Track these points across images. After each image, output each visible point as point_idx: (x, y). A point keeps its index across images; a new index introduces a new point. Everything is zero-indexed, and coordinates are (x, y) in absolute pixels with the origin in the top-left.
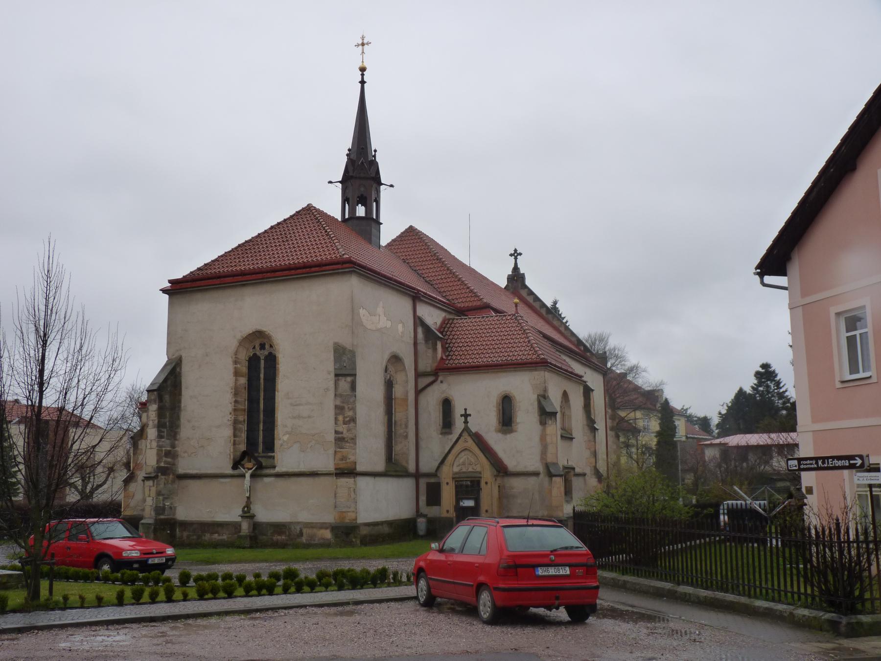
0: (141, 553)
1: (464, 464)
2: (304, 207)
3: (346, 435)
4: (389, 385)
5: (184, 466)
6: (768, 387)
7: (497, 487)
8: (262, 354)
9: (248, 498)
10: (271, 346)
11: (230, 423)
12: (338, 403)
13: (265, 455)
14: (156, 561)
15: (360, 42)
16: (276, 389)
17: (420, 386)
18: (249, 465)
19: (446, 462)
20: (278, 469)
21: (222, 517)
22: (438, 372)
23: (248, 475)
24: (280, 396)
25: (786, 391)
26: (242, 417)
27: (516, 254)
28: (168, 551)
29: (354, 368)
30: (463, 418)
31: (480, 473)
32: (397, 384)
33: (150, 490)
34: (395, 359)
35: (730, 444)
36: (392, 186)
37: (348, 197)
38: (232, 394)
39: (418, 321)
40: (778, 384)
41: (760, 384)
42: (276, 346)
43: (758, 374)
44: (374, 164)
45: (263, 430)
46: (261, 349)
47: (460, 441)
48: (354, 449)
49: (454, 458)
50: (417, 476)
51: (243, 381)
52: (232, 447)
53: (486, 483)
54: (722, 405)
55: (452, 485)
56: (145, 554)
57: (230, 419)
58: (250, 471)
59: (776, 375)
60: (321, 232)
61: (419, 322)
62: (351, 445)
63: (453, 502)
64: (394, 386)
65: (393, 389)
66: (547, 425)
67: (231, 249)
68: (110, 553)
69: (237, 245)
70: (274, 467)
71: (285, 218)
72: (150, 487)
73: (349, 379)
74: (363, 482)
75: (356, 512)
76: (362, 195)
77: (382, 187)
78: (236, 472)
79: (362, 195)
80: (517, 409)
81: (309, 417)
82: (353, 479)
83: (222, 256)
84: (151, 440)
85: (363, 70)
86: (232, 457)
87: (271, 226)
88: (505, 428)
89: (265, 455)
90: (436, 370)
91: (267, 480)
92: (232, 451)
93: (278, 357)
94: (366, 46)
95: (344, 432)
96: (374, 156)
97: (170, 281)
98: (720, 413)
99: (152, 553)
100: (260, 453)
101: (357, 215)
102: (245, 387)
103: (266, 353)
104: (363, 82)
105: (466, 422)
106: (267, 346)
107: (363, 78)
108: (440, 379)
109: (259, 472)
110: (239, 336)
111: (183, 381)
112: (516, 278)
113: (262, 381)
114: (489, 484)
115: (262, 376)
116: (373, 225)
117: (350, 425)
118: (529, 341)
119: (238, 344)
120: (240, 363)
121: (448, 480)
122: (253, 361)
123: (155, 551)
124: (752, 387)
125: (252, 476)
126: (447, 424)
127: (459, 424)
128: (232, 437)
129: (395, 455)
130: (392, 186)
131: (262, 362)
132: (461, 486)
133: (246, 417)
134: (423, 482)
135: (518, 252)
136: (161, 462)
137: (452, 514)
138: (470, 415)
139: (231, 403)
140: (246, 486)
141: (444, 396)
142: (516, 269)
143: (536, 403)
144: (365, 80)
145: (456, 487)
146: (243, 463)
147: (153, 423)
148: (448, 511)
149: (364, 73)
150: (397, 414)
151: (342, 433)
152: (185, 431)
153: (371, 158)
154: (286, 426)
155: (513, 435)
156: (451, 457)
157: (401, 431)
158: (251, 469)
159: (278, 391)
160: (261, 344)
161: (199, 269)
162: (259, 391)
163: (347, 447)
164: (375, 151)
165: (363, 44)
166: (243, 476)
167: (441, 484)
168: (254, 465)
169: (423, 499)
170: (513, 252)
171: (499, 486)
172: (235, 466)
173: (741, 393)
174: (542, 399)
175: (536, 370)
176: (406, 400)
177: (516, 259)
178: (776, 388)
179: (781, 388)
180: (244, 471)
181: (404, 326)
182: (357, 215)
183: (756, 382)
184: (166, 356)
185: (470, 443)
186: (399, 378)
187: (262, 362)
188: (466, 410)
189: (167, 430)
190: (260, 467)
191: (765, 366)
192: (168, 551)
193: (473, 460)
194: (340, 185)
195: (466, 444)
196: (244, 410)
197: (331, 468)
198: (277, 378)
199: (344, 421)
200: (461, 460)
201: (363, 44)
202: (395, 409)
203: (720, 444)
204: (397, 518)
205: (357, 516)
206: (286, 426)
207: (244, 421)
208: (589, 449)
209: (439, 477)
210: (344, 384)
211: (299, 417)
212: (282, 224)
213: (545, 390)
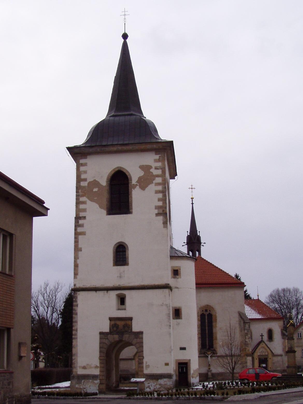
8: (206, 313)
10: (210, 311)
15: (191, 187)
31: (268, 355)
46: (205, 311)
53: (270, 359)
58: (210, 355)
70: (217, 354)
73: (248, 324)
85: (192, 199)
87: (218, 267)
103: (208, 313)
104: (192, 204)
105: (262, 338)
106: (208, 311)
107: (192, 202)
113: (207, 323)
121: (256, 358)
125: (211, 357)
138: (263, 336)
149: (193, 200)
160: (205, 310)
164: (199, 232)
165: (192, 188)
166: (208, 357)
188: (262, 334)
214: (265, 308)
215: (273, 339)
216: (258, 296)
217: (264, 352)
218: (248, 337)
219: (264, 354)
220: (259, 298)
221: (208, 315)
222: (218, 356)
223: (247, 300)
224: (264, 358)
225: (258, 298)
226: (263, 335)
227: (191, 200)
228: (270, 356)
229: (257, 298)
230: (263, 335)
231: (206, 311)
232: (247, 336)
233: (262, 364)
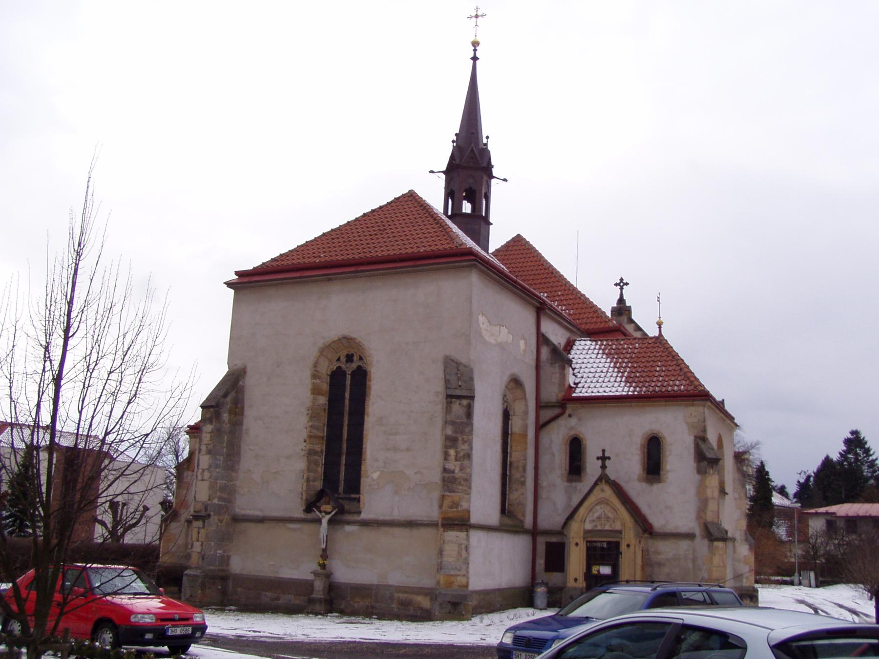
0: (157, 620)
2: (404, 193)
3: (458, 474)
4: (506, 416)
5: (244, 505)
6: (856, 454)
7: (641, 552)
9: (324, 550)
10: (361, 358)
11: (304, 453)
12: (449, 431)
13: (347, 496)
14: (179, 631)
15: (474, 14)
16: (366, 412)
17: (542, 420)
18: (328, 508)
19: (576, 516)
20: (364, 516)
21: (289, 572)
22: (565, 404)
23: (325, 521)
24: (370, 422)
25: (876, 459)
26: (319, 446)
27: (622, 284)
28: (196, 617)
29: (472, 389)
30: (600, 461)
31: (620, 532)
32: (514, 415)
33: (199, 533)
34: (516, 382)
35: (839, 514)
36: (505, 180)
37: (453, 189)
38: (308, 417)
39: (541, 339)
40: (867, 451)
41: (848, 452)
42: (368, 358)
43: (847, 442)
44: (485, 153)
45: (345, 465)
46: (347, 361)
47: (595, 492)
48: (468, 494)
49: (587, 511)
50: (534, 533)
51: (323, 400)
52: (305, 484)
53: (628, 546)
55: (583, 547)
56: (162, 620)
57: (304, 448)
58: (328, 517)
59: (866, 443)
60: (428, 221)
61: (542, 339)
62: (465, 488)
63: (583, 568)
64: (511, 417)
65: (510, 422)
66: (707, 475)
67: (313, 238)
68: (114, 617)
69: (321, 234)
70: (360, 513)
71: (381, 205)
72: (199, 528)
73: (465, 402)
74: (477, 538)
75: (466, 576)
76: (470, 188)
77: (493, 181)
78: (310, 516)
79: (470, 188)
81: (408, 450)
82: (465, 533)
83: (302, 246)
84: (203, 470)
85: (475, 44)
86: (304, 497)
88: (650, 476)
89: (347, 496)
90: (563, 400)
91: (348, 528)
92: (305, 489)
93: (370, 372)
94: (480, 18)
95: (456, 471)
96: (486, 145)
97: (237, 273)
98: (799, 482)
99: (173, 620)
100: (340, 494)
101: (464, 211)
102: (325, 410)
103: (354, 366)
104: (475, 59)
105: (604, 467)
106: (355, 358)
107: (475, 54)
108: (568, 412)
109: (339, 517)
110: (320, 343)
111: (246, 397)
112: (622, 309)
113: (347, 402)
114: (632, 547)
115: (347, 395)
116: (482, 223)
117: (464, 463)
118: (681, 369)
119: (319, 354)
122: (337, 376)
123: (177, 617)
124: (841, 454)
125: (330, 522)
127: (592, 468)
128: (306, 472)
129: (508, 505)
130: (505, 180)
131: (349, 377)
132: (595, 548)
133: (324, 447)
134: (542, 541)
135: (624, 281)
136: (214, 499)
137: (582, 584)
138: (609, 458)
139: (306, 428)
140: (322, 535)
141: (572, 433)
142: (621, 300)
143: (692, 446)
144: (477, 56)
145: (588, 549)
146: (318, 504)
147: (207, 447)
148: (576, 580)
149: (477, 48)
151: (453, 472)
152: (247, 462)
153: (482, 146)
154: (377, 460)
155: (660, 485)
156: (582, 510)
157: (516, 475)
158: (329, 513)
159: (368, 416)
161: (273, 260)
162: (342, 415)
163: (460, 491)
164: (487, 138)
165: (477, 16)
167: (566, 545)
168: (334, 508)
169: (541, 562)
170: (618, 281)
171: (642, 551)
172: (309, 509)
173: (827, 462)
174: (700, 442)
175: (693, 405)
176: (525, 436)
177: (622, 289)
178: (865, 455)
179: (871, 455)
180: (321, 516)
181: (526, 343)
182: (464, 211)
183: (845, 448)
184: (227, 365)
185: (608, 492)
186: (518, 408)
187: (349, 377)
188: (604, 451)
189: (223, 457)
190: (342, 511)
191: (855, 433)
192: (196, 617)
193: (610, 515)
194: (443, 176)
195: (602, 495)
196: (323, 438)
197: (434, 513)
198: (367, 399)
199: (456, 456)
200: (596, 515)
201: (477, 16)
202: (511, 447)
203: (827, 513)
204: (510, 585)
205: (468, 583)
206: (377, 460)
207: (322, 452)
208: (740, 509)
209: (566, 535)
210: (458, 408)
211: (395, 449)
212: (377, 212)
213: (704, 430)
214: (663, 363)
215: (662, 473)
216: (660, 325)
217: (608, 518)
218: (456, 452)
219: (607, 528)
220: (663, 333)
221: (353, 374)
222: (366, 524)
223: (617, 340)
224: (608, 543)
225: (660, 331)
226: (606, 455)
227: (473, 48)
228: (630, 536)
229: (657, 334)
230: (606, 455)
231: (350, 358)
232: (456, 448)
233: (600, 564)
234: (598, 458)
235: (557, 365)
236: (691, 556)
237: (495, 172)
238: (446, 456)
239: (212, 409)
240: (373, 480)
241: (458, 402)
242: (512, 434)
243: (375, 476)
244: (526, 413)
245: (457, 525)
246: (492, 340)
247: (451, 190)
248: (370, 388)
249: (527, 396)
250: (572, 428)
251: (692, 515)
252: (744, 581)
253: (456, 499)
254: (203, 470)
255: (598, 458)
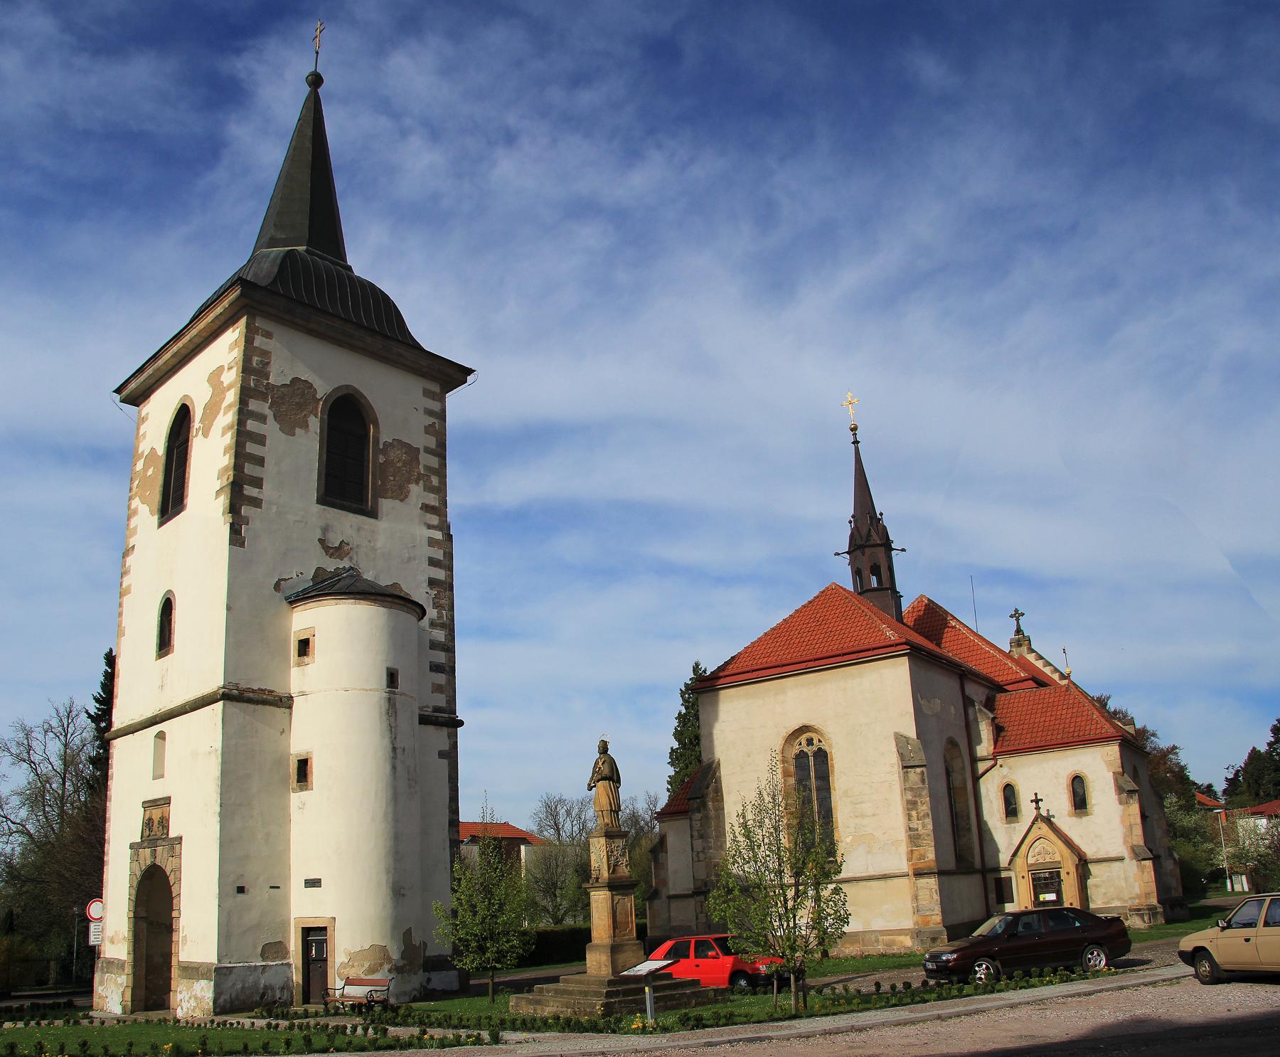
1: (1039, 854)
8: (809, 750)
20: (843, 875)
36: (903, 550)
46: (808, 745)
53: (1068, 873)
54: (1227, 769)
80: (1091, 790)
81: (874, 815)
104: (856, 442)
105: (1038, 808)
108: (1000, 762)
120: (787, 762)
126: (1011, 811)
127: (1027, 811)
130: (903, 550)
131: (811, 759)
132: (1039, 879)
141: (1005, 781)
150: (957, 805)
156: (1024, 847)
160: (807, 740)
164: (881, 514)
173: (1254, 754)
177: (1018, 620)
187: (811, 759)
188: (1036, 794)
195: (1040, 833)
200: (1037, 850)
211: (863, 816)
234: (1032, 801)
235: (984, 722)
236: (1123, 876)
237: (893, 546)
238: (909, 817)
239: (698, 800)
240: (847, 844)
241: (912, 770)
242: (954, 788)
243: (848, 840)
244: (963, 769)
245: (926, 874)
246: (930, 713)
247: (858, 568)
248: (833, 766)
249: (963, 754)
250: (1005, 777)
251: (1120, 841)
252: (1173, 892)
253: (922, 852)
254: (698, 853)
255: (1032, 801)
